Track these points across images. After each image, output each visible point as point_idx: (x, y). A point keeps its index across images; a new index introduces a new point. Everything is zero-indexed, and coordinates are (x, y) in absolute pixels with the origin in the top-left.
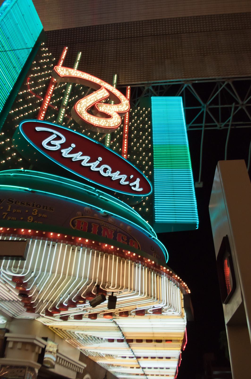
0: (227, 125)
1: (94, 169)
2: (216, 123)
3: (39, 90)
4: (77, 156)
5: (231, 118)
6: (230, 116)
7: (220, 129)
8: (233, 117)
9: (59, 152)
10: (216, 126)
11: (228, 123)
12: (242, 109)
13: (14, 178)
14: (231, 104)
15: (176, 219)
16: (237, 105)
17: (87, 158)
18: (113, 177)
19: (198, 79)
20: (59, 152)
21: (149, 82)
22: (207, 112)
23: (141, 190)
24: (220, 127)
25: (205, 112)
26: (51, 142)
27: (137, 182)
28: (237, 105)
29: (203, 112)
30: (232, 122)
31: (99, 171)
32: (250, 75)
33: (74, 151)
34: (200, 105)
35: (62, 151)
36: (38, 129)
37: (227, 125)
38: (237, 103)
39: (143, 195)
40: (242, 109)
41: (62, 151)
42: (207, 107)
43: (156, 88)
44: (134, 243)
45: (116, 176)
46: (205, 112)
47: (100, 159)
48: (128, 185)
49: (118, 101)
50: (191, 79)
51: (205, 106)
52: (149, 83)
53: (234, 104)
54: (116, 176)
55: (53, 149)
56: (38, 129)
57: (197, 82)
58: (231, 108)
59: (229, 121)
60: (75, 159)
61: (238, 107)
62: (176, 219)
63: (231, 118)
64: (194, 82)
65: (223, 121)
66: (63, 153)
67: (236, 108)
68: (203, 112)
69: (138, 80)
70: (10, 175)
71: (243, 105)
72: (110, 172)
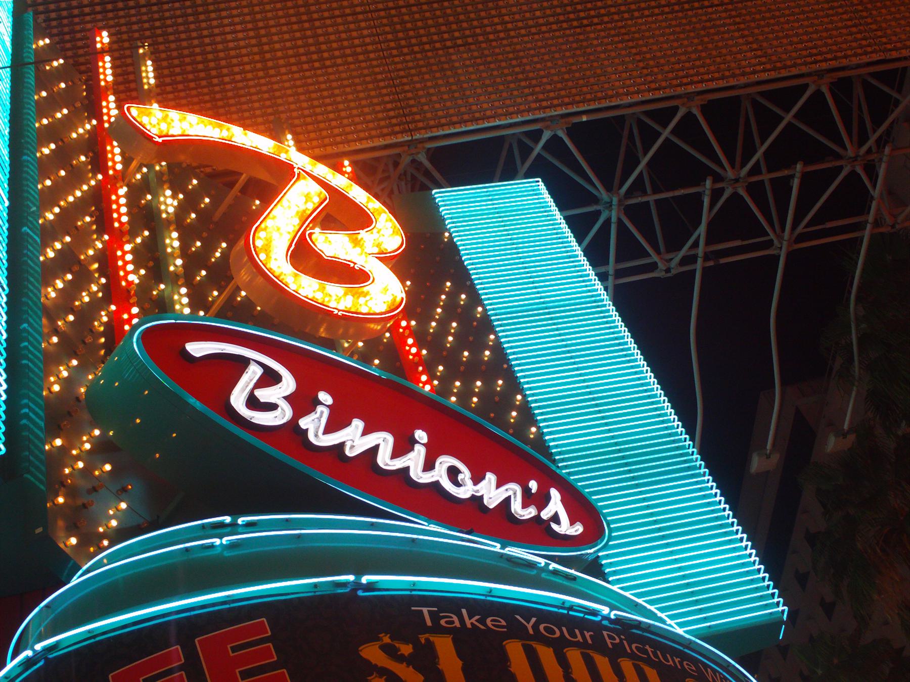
0: (690, 259)
1: (387, 465)
2: (655, 258)
3: (80, 207)
4: (354, 438)
5: (702, 229)
6: (700, 223)
7: (669, 275)
8: (710, 225)
9: (292, 430)
10: (653, 267)
11: (692, 252)
12: (735, 195)
13: (227, 554)
14: (700, 181)
15: (705, 620)
16: (719, 185)
17: (384, 441)
18: (348, 445)
19: (584, 110)
20: (292, 430)
21: (417, 136)
22: (619, 221)
23: (578, 529)
24: (668, 270)
25: (614, 219)
26: (259, 393)
27: (555, 504)
28: (719, 185)
29: (608, 222)
30: (707, 243)
31: (437, 482)
32: (905, 53)
33: (335, 424)
34: (595, 200)
35: (304, 423)
36: (197, 349)
37: (690, 259)
38: (718, 178)
39: (591, 548)
40: (735, 195)
41: (304, 423)
42: (620, 201)
43: (436, 156)
44: (446, 622)
45: (491, 492)
46: (614, 219)
47: (421, 435)
48: (537, 518)
49: (359, 220)
50: (564, 111)
51: (615, 200)
52: (416, 140)
53: (708, 183)
54: (491, 492)
55: (333, 440)
56: (197, 349)
57: (584, 119)
58: (698, 197)
59: (696, 245)
60: (352, 447)
61: (722, 190)
62: (705, 620)
63: (702, 229)
64: (576, 120)
65: (674, 245)
66: (307, 430)
67: (716, 194)
68: (608, 222)
69: (362, 135)
70: (212, 546)
71: (737, 180)
72: (469, 482)
